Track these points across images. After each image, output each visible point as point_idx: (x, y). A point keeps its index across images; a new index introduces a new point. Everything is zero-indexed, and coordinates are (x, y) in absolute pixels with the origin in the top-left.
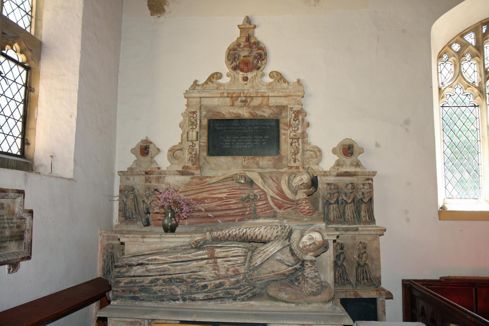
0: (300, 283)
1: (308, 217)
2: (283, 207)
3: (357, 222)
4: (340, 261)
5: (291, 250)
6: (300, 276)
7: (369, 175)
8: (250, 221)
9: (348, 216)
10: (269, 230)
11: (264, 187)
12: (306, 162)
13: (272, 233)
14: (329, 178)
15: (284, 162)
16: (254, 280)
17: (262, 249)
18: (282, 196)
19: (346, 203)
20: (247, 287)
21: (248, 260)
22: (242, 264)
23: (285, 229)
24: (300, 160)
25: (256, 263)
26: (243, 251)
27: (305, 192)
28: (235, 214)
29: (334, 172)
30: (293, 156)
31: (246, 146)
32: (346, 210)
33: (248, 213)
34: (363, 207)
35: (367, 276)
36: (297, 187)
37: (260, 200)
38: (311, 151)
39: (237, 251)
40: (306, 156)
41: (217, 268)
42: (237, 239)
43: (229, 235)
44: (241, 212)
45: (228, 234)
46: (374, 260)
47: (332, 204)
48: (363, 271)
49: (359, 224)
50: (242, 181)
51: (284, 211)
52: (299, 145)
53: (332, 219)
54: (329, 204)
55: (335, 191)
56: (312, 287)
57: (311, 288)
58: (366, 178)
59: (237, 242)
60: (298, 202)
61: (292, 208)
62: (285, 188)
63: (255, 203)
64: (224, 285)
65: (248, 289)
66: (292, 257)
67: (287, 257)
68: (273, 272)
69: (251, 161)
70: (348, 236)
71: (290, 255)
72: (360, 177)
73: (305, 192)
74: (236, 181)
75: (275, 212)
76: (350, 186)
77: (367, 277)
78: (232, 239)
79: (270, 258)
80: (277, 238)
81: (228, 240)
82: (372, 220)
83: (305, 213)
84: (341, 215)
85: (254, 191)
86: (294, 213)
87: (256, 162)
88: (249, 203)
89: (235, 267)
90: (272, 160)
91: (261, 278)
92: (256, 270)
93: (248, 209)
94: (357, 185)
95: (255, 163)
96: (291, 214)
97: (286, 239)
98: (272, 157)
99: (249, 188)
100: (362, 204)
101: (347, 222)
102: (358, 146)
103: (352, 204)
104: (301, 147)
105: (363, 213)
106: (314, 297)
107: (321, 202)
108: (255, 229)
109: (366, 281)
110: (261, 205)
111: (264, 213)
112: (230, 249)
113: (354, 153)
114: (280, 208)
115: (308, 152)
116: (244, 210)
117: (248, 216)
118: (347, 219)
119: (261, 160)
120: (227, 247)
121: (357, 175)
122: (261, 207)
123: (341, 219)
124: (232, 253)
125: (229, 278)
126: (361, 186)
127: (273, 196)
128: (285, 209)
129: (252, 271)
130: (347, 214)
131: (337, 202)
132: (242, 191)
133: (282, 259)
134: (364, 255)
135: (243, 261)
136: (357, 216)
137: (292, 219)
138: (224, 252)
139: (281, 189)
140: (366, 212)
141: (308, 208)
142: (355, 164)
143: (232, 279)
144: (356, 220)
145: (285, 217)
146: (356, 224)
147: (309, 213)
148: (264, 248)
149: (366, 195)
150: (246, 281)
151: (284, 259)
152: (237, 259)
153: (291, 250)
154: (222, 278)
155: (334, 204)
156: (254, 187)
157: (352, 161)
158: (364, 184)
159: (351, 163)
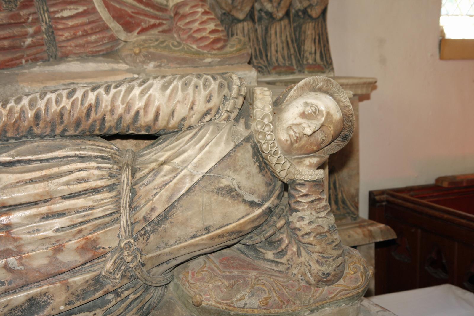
0: (282, 253)
1: (214, 52)
2: (138, 25)
3: (295, 67)
5: (257, 152)
6: (282, 230)
8: (38, 69)
10: (180, 92)
13: (193, 103)
16: (149, 266)
17: (162, 159)
20: (126, 293)
21: (125, 201)
22: (107, 219)
23: (230, 88)
25: (153, 209)
26: (104, 172)
32: (273, 37)
33: (29, 41)
34: (309, 29)
39: (83, 174)
41: (11, 247)
42: (65, 130)
43: (37, 116)
45: (30, 114)
47: (239, 21)
49: (300, 71)
51: (143, 37)
54: (232, 22)
56: (324, 260)
57: (322, 264)
59: (67, 141)
60: (181, 11)
61: (160, 29)
63: (52, 10)
64: (46, 304)
65: (130, 300)
66: (260, 175)
67: (248, 178)
68: (208, 229)
71: (254, 169)
75: (114, 40)
78: (48, 131)
79: (198, 187)
80: (208, 118)
81: (30, 134)
83: (206, 43)
84: (260, 49)
86: (176, 43)
88: (31, 10)
89: (85, 233)
91: (167, 254)
92: (153, 232)
93: (31, 30)
97: (237, 120)
106: (326, 288)
108: (129, 90)
111: (81, 41)
112: (55, 170)
114: (128, 27)
116: (16, 31)
118: (274, 59)
120: (36, 161)
122: (70, 23)
123: (261, 61)
124: (68, 183)
125: (65, 276)
129: (141, 239)
131: (251, 16)
133: (234, 185)
135: (111, 208)
136: (295, 51)
137: (171, 60)
138: (32, 181)
141: (211, 26)
143: (76, 279)
144: (294, 62)
145: (153, 54)
146: (293, 73)
148: (167, 154)
150: (123, 277)
151: (242, 185)
152: (90, 203)
153: (257, 152)
154: (37, 282)
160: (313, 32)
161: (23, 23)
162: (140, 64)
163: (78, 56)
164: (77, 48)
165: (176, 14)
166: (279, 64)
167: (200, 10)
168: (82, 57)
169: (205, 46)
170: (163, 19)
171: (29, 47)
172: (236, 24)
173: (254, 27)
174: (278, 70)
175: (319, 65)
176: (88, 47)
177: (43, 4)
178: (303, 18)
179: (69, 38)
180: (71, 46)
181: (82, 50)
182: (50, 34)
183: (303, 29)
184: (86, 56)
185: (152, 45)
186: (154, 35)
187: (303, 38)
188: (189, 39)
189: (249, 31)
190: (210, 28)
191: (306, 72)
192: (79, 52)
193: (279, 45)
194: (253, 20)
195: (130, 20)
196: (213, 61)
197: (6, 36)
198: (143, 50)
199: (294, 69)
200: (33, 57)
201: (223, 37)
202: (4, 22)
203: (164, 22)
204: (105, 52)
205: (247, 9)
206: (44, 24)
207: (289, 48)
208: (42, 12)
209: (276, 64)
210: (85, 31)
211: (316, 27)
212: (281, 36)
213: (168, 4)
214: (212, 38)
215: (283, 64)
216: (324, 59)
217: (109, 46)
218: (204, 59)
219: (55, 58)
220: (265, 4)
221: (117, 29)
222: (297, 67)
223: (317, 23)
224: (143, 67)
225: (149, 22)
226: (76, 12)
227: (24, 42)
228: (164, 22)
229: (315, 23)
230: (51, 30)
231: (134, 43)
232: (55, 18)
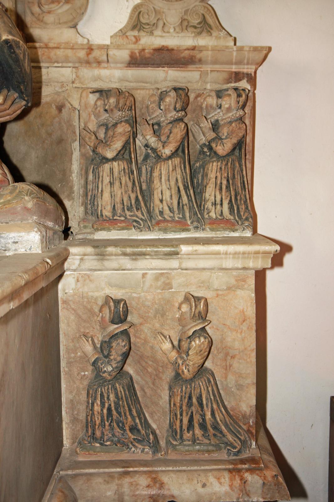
3: (189, 222)
4: (109, 363)
9: (161, 201)
12: (33, 14)
14: (104, 72)
19: (159, 158)
29: (118, 47)
32: (156, 181)
34: (213, 170)
35: (203, 416)
46: (233, 357)
47: (107, 160)
48: (190, 398)
49: (197, 228)
53: (107, 212)
54: (102, 160)
55: (118, 114)
58: (231, 73)
70: (144, 275)
72: (208, 68)
76: (170, 99)
77: (204, 420)
82: (243, 210)
84: (137, 197)
94: (198, 96)
100: (209, 162)
101: (158, 223)
103: (177, 161)
105: (210, 193)
107: (76, 155)
109: (198, 432)
123: (139, 214)
126: (212, 101)
130: (157, 196)
134: (197, 343)
136: (190, 200)
140: (221, 189)
142: (195, 21)
144: (187, 215)
146: (188, 230)
149: (224, 131)
155: (114, 159)
157: (186, 12)
158: (219, 94)
159: (183, 20)
160: (219, 175)
172: (104, 163)
175: (228, 221)
199: (188, 225)
215: (170, 217)
229: (222, 163)
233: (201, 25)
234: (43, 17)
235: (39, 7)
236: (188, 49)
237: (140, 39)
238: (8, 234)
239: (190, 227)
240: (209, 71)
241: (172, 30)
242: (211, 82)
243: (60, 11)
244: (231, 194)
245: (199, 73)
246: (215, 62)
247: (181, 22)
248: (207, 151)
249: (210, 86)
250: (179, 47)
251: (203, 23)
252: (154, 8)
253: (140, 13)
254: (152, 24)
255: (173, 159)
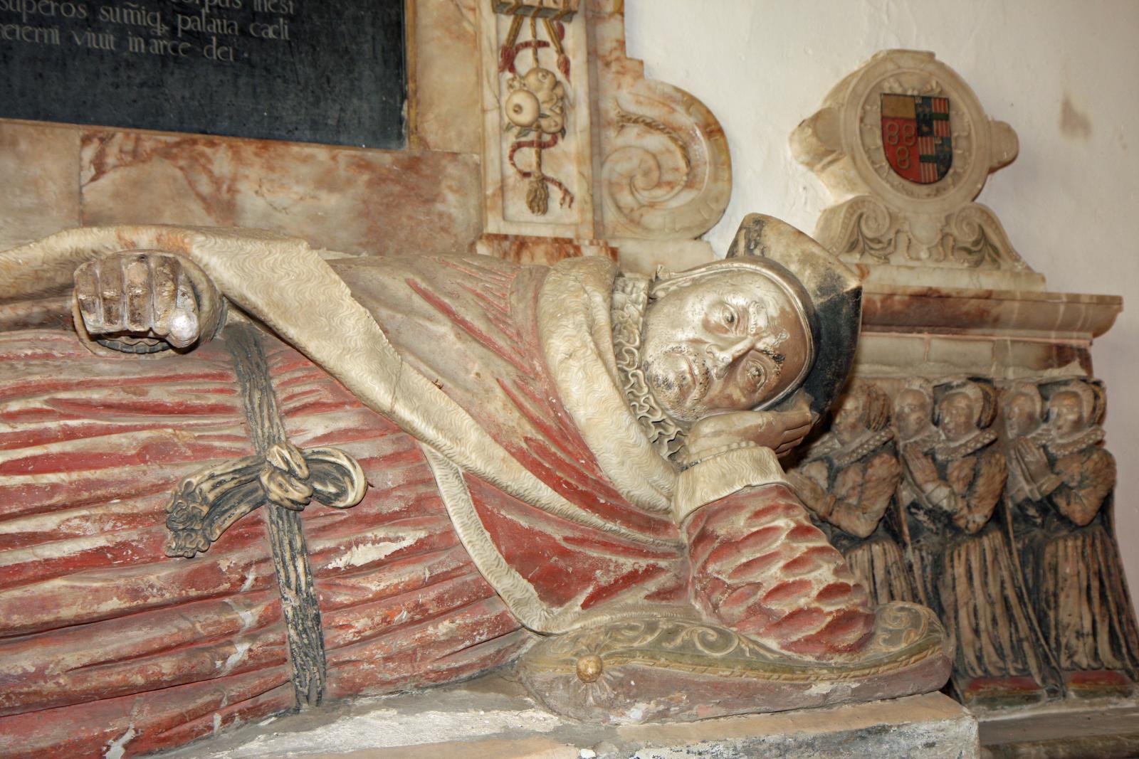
1: (838, 659)
2: (586, 578)
3: (1038, 681)
7: (1067, 326)
11: (396, 383)
12: (619, 208)
15: (452, 204)
18: (559, 463)
24: (577, 189)
27: (760, 438)
28: (96, 680)
30: (527, 157)
31: (108, 41)
32: (962, 586)
33: (240, 652)
34: (1068, 559)
36: (695, 393)
37: (363, 520)
38: (651, 125)
40: (618, 166)
44: (165, 650)
49: (1053, 692)
50: (183, 325)
51: (602, 618)
52: (565, 66)
58: (1050, 346)
60: (722, 529)
61: (652, 586)
62: (589, 396)
63: (318, 545)
69: (163, 172)
72: (1005, 335)
73: (760, 438)
74: (110, 316)
75: (507, 628)
83: (812, 631)
85: (292, 423)
86: (712, 636)
87: (205, 187)
90: (349, 182)
93: (248, 617)
95: (202, 198)
96: (687, 645)
98: (344, 154)
99: (237, 402)
102: (978, 109)
104: (578, 85)
110: (376, 565)
111: (403, 641)
113: (956, 162)
114: (554, 586)
115: (632, 132)
116: (202, 622)
117: (235, 689)
119: (255, 171)
121: (996, 322)
122: (374, 585)
127: (490, 470)
128: (601, 595)
131: (889, 526)
132: (167, 429)
136: (1032, 629)
139: (553, 402)
141: (823, 574)
142: (968, 239)
144: (1032, 663)
146: (1032, 699)
147: (843, 621)
156: (286, 382)
159: (945, 236)
161: (226, 593)
162: (598, 710)
163: (392, 689)
164: (391, 665)
165: (703, 537)
166: (986, 671)
167: (784, 523)
168: (402, 692)
169: (808, 640)
170: (655, 555)
171: (241, 670)
173: (901, 557)
174: (985, 690)
176: (423, 658)
177: (290, 531)
178: (1043, 525)
179: (368, 633)
180: (370, 660)
181: (406, 670)
182: (309, 624)
183: (1048, 557)
184: (417, 687)
185: (636, 645)
186: (634, 607)
187: (1050, 585)
188: (753, 619)
189: (888, 572)
190: (820, 582)
191: (1072, 695)
192: (396, 676)
193: (981, 613)
194: (897, 538)
195: (561, 564)
196: (834, 691)
197: (167, 641)
198: (607, 664)
199: (1037, 687)
200: (248, 704)
201: (861, 610)
202: (168, 596)
203: (662, 563)
204: (476, 671)
205: (880, 505)
206: (290, 594)
207: (1011, 619)
208: (288, 556)
209: (979, 673)
210: (418, 606)
211: (1088, 550)
212: (985, 584)
213: (673, 506)
214: (831, 613)
216: (1124, 650)
217: (490, 650)
218: (808, 686)
219: (319, 701)
220: (929, 487)
221: (518, 595)
222: (1044, 680)
223: (1088, 541)
224: (607, 719)
225: (617, 566)
226: (395, 547)
227: (225, 659)
228: (662, 563)
229: (1084, 541)
230: (312, 612)
231: (575, 640)
232: (328, 573)
233: (979, 247)
234: (641, 216)
235: (632, 193)
236: (977, 297)
237: (868, 272)
238: (915, 725)
239: (1039, 692)
240: (1009, 343)
241: (924, 255)
242: (1015, 365)
243: (674, 204)
244: (1109, 610)
245: (990, 345)
246: (1021, 325)
247: (942, 239)
248: (1037, 515)
249: (1014, 372)
250: (960, 292)
251: (983, 242)
252: (887, 209)
253: (861, 216)
254: (885, 240)
255: (991, 536)
